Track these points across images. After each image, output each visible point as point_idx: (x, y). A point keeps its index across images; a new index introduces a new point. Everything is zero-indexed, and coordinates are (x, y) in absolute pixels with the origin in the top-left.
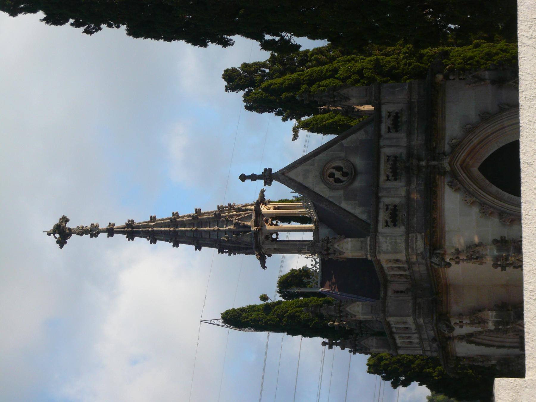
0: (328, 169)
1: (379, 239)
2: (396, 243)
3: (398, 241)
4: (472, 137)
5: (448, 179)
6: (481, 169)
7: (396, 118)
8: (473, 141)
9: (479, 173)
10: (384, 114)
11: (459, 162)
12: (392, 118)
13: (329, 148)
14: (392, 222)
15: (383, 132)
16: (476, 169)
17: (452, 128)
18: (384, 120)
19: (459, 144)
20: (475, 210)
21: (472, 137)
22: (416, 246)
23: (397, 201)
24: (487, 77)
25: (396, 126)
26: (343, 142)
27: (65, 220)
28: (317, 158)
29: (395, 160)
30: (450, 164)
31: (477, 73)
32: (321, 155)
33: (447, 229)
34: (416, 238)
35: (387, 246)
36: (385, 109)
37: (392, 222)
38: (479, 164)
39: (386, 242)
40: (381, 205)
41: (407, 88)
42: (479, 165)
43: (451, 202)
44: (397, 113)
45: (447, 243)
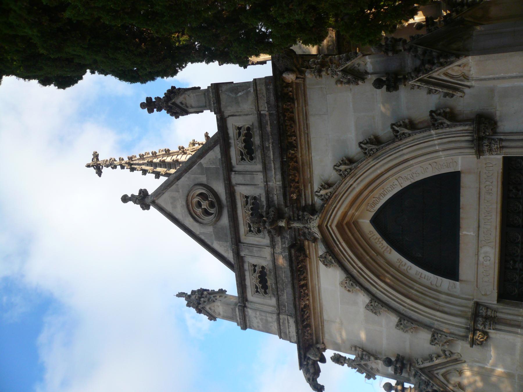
0: (193, 198)
1: (248, 312)
2: (267, 320)
3: (270, 319)
4: (351, 182)
5: (321, 250)
6: (375, 221)
7: (247, 135)
8: (354, 188)
9: (372, 229)
10: (232, 132)
11: (335, 222)
12: (242, 138)
13: (190, 169)
14: (262, 287)
15: (234, 161)
16: (368, 221)
17: (322, 163)
18: (232, 141)
19: (330, 198)
20: (363, 299)
21: (351, 182)
22: (289, 332)
23: (264, 263)
24: (370, 68)
25: (248, 153)
26: (202, 161)
27: (96, 156)
28: (180, 182)
29: (253, 203)
30: (320, 227)
31: (349, 63)
32: (183, 179)
33: (325, 317)
34: (288, 323)
35: (258, 322)
36: (232, 123)
37: (262, 287)
38: (372, 214)
39: (256, 317)
40: (246, 266)
41: (252, 91)
42: (371, 214)
43: (328, 281)
44: (248, 129)
45: (327, 336)
